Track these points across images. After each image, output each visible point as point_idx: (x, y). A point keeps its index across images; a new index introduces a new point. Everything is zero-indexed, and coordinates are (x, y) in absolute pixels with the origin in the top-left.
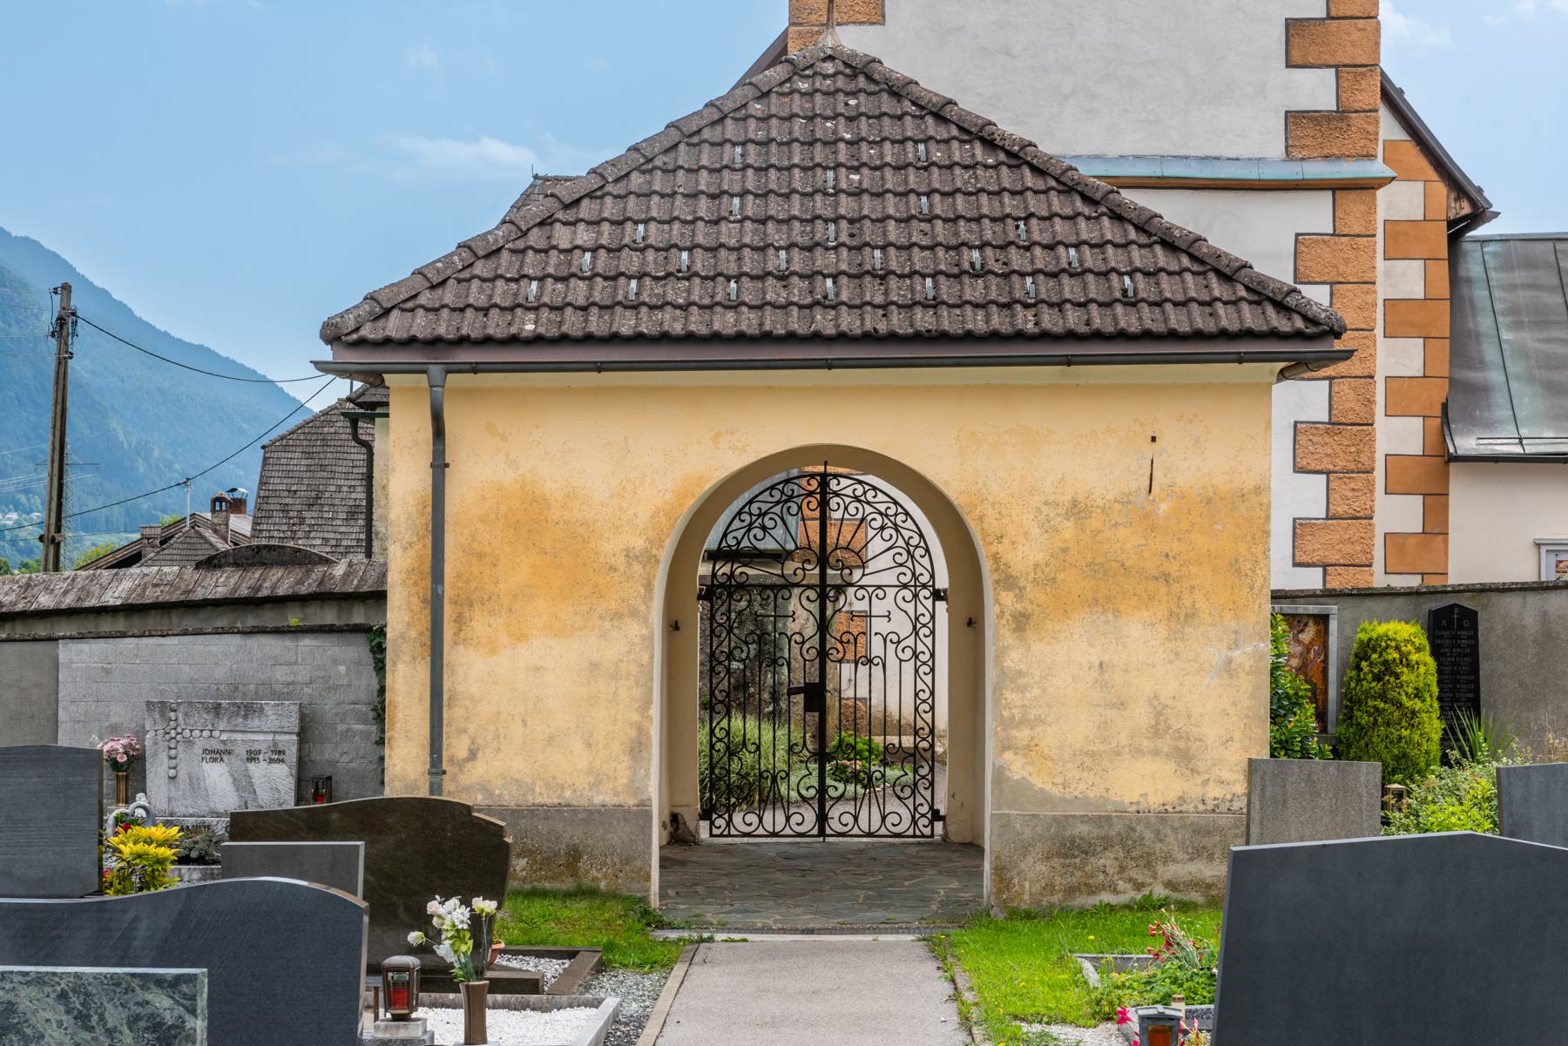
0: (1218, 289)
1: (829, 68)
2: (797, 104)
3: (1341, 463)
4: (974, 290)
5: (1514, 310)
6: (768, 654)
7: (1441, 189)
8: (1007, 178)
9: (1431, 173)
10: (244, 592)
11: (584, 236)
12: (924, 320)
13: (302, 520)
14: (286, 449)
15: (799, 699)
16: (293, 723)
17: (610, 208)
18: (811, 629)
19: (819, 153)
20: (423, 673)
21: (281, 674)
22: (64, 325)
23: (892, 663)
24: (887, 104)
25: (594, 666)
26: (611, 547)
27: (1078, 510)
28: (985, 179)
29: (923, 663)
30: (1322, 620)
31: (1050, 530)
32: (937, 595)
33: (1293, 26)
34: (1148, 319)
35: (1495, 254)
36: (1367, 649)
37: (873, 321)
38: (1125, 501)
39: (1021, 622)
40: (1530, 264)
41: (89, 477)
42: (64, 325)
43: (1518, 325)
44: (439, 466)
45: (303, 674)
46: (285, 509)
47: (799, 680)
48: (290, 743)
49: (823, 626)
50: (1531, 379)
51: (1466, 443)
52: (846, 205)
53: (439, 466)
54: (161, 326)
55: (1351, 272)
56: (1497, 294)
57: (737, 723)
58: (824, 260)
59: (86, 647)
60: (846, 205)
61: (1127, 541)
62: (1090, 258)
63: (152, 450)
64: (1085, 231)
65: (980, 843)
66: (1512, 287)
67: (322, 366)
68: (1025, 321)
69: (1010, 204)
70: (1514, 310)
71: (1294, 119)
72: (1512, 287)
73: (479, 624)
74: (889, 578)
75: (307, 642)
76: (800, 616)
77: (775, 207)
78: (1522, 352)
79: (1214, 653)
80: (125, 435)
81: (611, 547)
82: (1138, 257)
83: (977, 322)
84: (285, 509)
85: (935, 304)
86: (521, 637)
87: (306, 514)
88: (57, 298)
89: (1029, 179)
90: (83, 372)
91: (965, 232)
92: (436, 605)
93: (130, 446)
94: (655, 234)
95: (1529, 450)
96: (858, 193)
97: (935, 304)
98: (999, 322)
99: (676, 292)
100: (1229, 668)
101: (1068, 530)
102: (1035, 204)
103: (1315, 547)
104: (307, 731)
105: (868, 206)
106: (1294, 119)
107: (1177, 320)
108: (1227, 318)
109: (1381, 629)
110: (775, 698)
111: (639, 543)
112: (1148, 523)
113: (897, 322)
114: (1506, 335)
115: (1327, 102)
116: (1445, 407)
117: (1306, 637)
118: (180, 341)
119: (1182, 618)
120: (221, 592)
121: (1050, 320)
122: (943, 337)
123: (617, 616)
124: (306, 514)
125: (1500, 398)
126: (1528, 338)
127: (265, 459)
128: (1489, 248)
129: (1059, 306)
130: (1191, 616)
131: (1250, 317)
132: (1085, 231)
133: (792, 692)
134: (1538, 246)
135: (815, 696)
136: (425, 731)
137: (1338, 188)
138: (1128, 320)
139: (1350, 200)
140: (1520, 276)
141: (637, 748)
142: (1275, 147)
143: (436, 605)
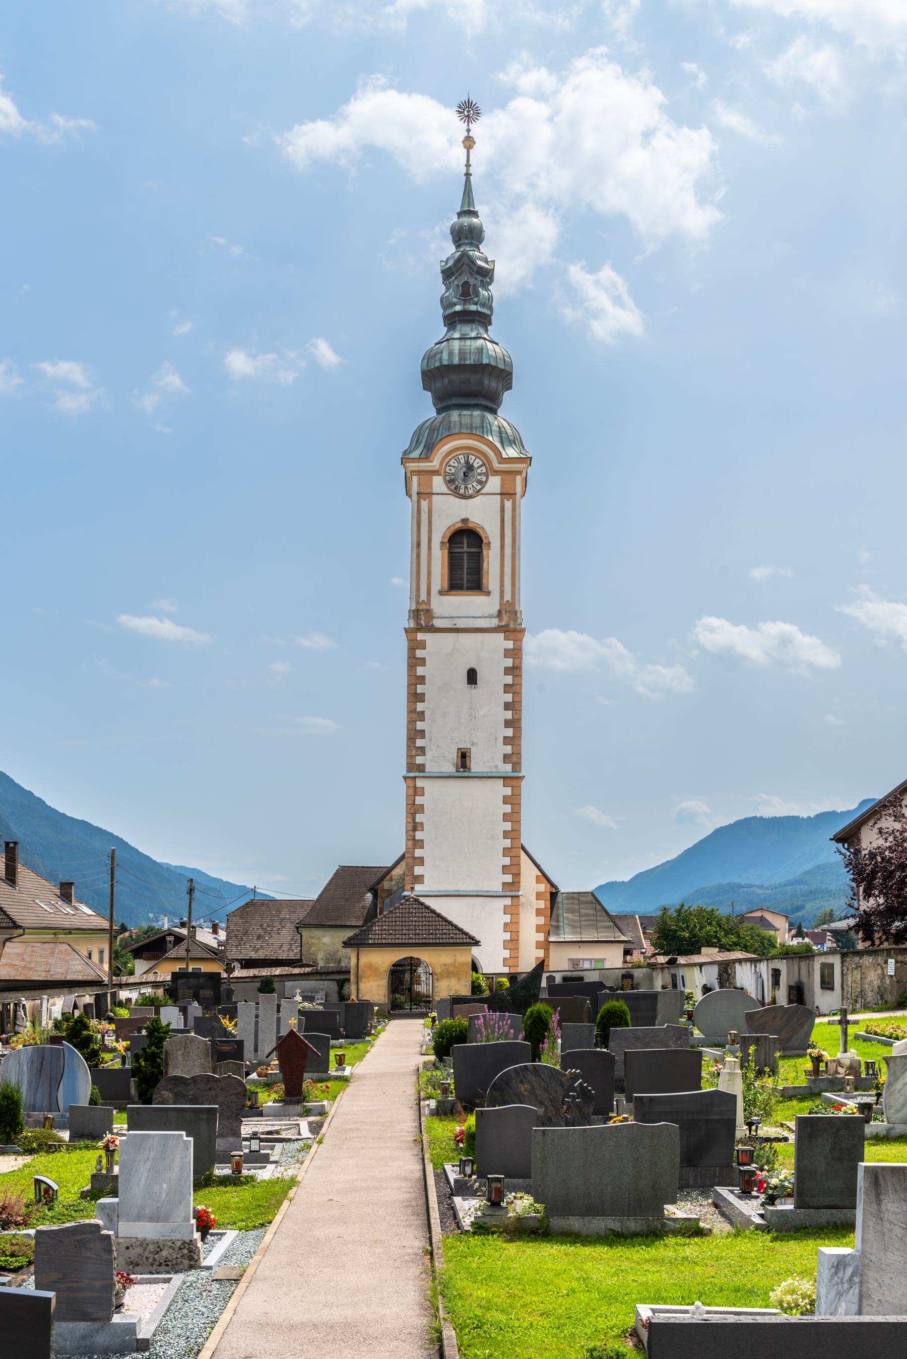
0: (464, 937)
1: (412, 900)
2: (407, 906)
3: (512, 948)
4: (431, 936)
5: (567, 909)
6: (401, 982)
7: (548, 885)
8: (437, 919)
9: (546, 882)
10: (302, 972)
11: (377, 928)
12: (424, 941)
13: (242, 940)
14: (235, 916)
15: (407, 991)
16: (325, 994)
17: (380, 924)
18: (409, 979)
19: (410, 915)
20: (356, 986)
21: (322, 987)
22: (191, 891)
23: (422, 985)
24: (420, 907)
25: (379, 985)
26: (381, 970)
27: (445, 965)
28: (434, 919)
29: (428, 985)
30: (493, 978)
31: (441, 968)
32: (430, 974)
33: (504, 867)
34: (454, 941)
35: (565, 896)
36: (499, 982)
37: (417, 941)
38: (452, 964)
39: (437, 980)
40: (572, 898)
41: (200, 934)
42: (191, 891)
43: (568, 913)
44: (358, 960)
45: (325, 986)
46: (236, 936)
47: (407, 987)
48: (324, 997)
49: (411, 979)
50: (569, 924)
51: (552, 938)
52: (414, 923)
53: (358, 960)
54: (61, 810)
55: (514, 912)
56: (564, 905)
57: (397, 995)
58: (411, 932)
59: (290, 983)
60: (414, 923)
61: (452, 969)
62: (447, 932)
63: (59, 875)
64: (447, 927)
65: (311, 904)
66: (568, 904)
67: (343, 947)
68: (438, 941)
69: (437, 923)
70: (567, 909)
71: (504, 884)
72: (568, 904)
73: (363, 980)
74: (422, 971)
75: (326, 982)
76: (407, 977)
77: (404, 924)
78: (568, 919)
79: (464, 983)
80: (44, 867)
81: (381, 970)
82: (454, 932)
83: (431, 941)
84: (236, 936)
85: (425, 938)
86: (369, 982)
87: (244, 938)
88: (189, 883)
89: (440, 919)
90: (20, 835)
91: (431, 928)
92: (357, 977)
93: (46, 873)
94: (387, 928)
95: (566, 940)
96: (415, 921)
97: (425, 938)
98: (434, 941)
99: (390, 937)
100: (466, 985)
101: (444, 967)
102: (441, 923)
103: (507, 963)
104: (326, 995)
105: (417, 923)
106: (504, 884)
107: (458, 941)
108: (465, 941)
109: (500, 979)
110: (403, 991)
111: (385, 969)
112: (455, 966)
113: (420, 941)
114: (565, 915)
115: (510, 880)
116: (549, 931)
117: (490, 980)
118: (18, 786)
119: (459, 979)
120: (297, 972)
121: (441, 941)
122: (426, 943)
123: (382, 979)
124: (244, 938)
125: (562, 929)
126: (570, 916)
127: (228, 919)
128: (564, 895)
129: (443, 939)
130: (460, 979)
131: (468, 941)
132: (447, 927)
133: (406, 989)
134: (575, 895)
135: (410, 990)
136: (356, 994)
137: (512, 897)
138: (451, 941)
139: (515, 899)
140: (570, 901)
141: (385, 996)
142: (500, 889)
143: (357, 977)
